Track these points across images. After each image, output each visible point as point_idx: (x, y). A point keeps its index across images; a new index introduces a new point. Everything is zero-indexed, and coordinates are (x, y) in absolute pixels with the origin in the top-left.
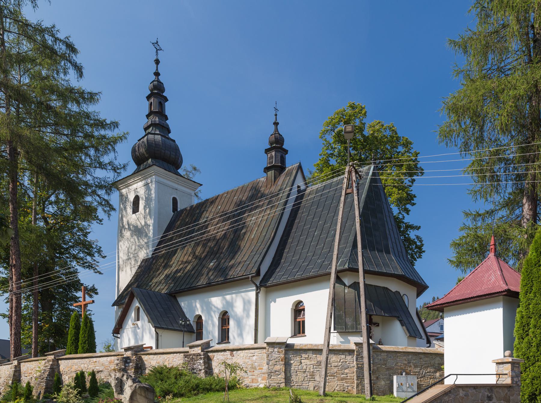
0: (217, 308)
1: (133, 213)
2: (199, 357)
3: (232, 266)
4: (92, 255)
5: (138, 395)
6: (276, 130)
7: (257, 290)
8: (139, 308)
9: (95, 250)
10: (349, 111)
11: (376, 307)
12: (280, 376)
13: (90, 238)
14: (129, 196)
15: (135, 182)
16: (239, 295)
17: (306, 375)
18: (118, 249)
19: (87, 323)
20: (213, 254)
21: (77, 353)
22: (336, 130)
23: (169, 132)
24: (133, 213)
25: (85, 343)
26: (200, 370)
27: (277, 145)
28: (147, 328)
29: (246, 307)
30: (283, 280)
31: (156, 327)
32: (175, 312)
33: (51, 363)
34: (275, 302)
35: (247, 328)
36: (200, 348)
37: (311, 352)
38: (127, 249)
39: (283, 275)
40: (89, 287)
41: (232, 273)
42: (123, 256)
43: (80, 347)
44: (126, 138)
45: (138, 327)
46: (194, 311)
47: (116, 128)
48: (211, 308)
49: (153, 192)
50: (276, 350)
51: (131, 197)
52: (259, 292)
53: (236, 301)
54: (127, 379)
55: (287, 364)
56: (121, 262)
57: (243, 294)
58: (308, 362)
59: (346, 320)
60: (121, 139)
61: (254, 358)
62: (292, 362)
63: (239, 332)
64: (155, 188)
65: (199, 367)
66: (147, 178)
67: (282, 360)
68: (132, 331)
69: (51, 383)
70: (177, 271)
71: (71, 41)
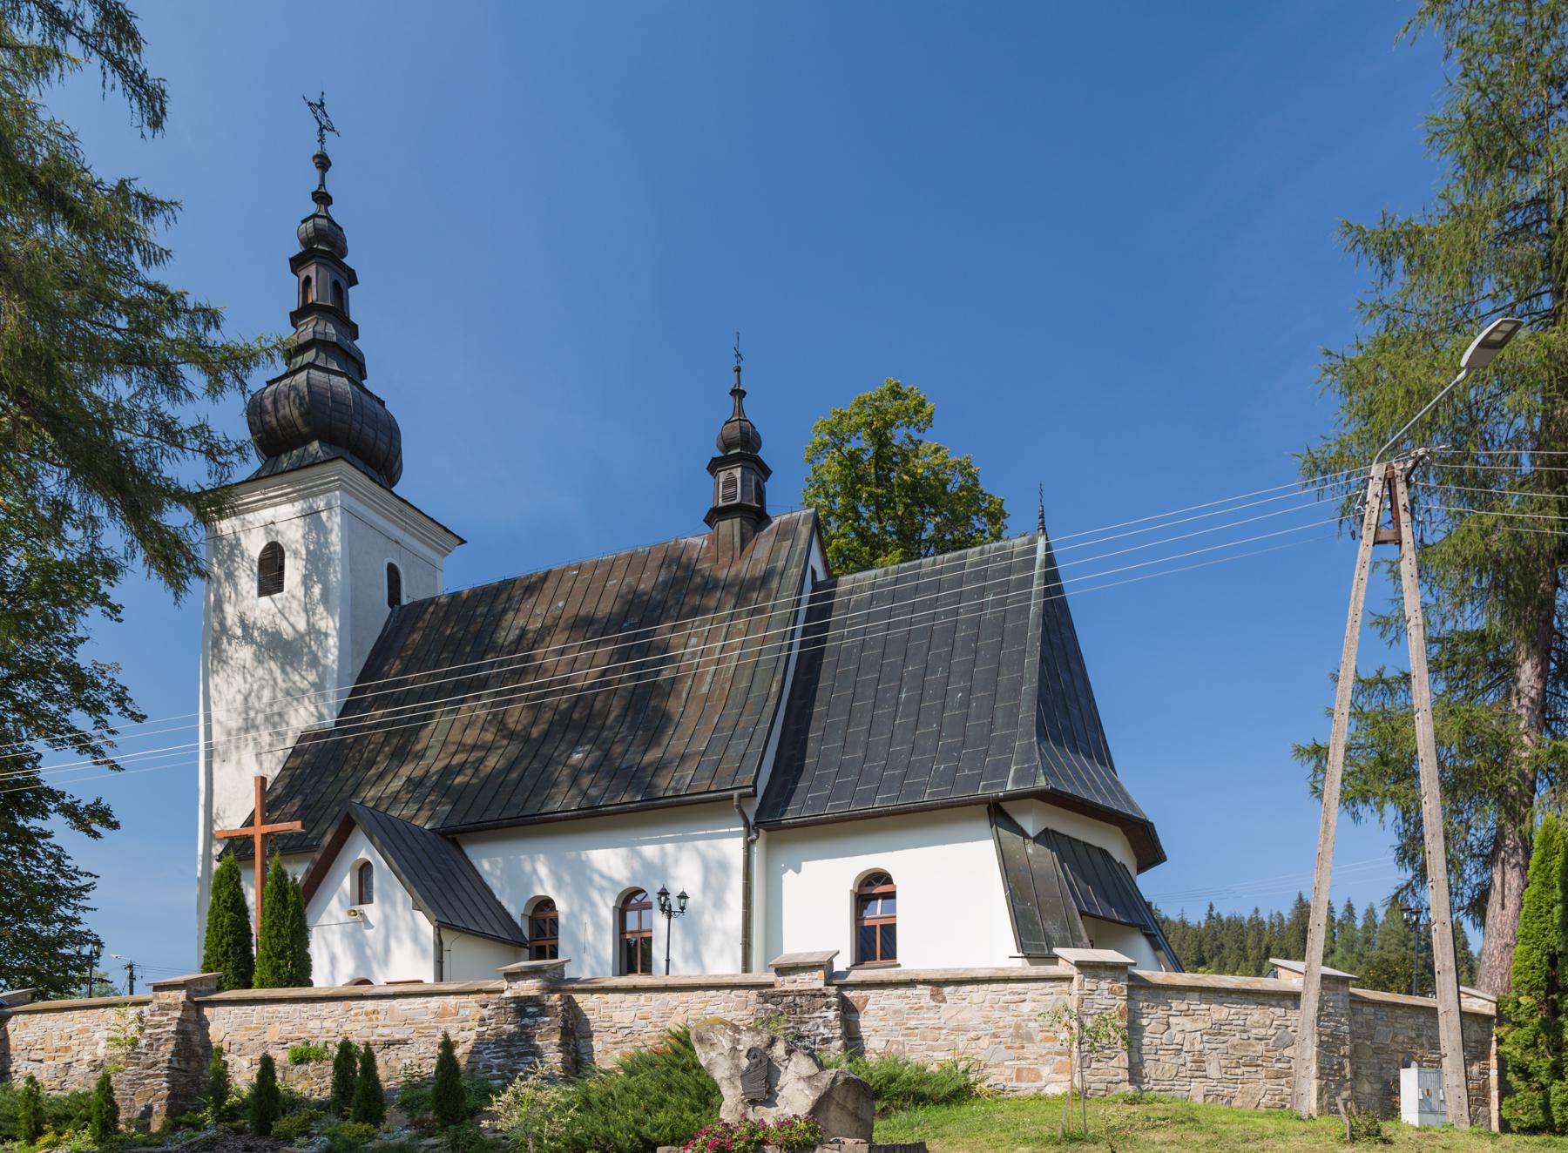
0: (611, 880)
1: (260, 595)
2: (820, 1001)
4: (95, 708)
5: (833, 1108)
9: (108, 694)
12: (1114, 1062)
14: (244, 542)
16: (689, 845)
17: (1181, 1061)
19: (286, 891)
21: (249, 985)
22: (845, 450)
24: (260, 595)
26: (826, 1041)
27: (743, 449)
28: (402, 924)
29: (713, 881)
30: (829, 810)
31: (440, 926)
33: (178, 1014)
34: (798, 870)
35: (717, 939)
36: (820, 974)
37: (1196, 995)
38: (240, 698)
39: (828, 798)
40: (82, 805)
41: (665, 784)
45: (366, 920)
46: (530, 886)
47: (213, 329)
48: (591, 881)
49: (335, 538)
50: (1104, 985)
51: (254, 545)
52: (753, 841)
53: (676, 861)
54: (789, 1052)
55: (1133, 1032)
56: (218, 735)
57: (701, 844)
58: (1187, 1024)
61: (1026, 1008)
63: (689, 948)
64: (342, 527)
65: (822, 1030)
66: (315, 495)
68: (343, 934)
69: (184, 1080)
70: (448, 771)
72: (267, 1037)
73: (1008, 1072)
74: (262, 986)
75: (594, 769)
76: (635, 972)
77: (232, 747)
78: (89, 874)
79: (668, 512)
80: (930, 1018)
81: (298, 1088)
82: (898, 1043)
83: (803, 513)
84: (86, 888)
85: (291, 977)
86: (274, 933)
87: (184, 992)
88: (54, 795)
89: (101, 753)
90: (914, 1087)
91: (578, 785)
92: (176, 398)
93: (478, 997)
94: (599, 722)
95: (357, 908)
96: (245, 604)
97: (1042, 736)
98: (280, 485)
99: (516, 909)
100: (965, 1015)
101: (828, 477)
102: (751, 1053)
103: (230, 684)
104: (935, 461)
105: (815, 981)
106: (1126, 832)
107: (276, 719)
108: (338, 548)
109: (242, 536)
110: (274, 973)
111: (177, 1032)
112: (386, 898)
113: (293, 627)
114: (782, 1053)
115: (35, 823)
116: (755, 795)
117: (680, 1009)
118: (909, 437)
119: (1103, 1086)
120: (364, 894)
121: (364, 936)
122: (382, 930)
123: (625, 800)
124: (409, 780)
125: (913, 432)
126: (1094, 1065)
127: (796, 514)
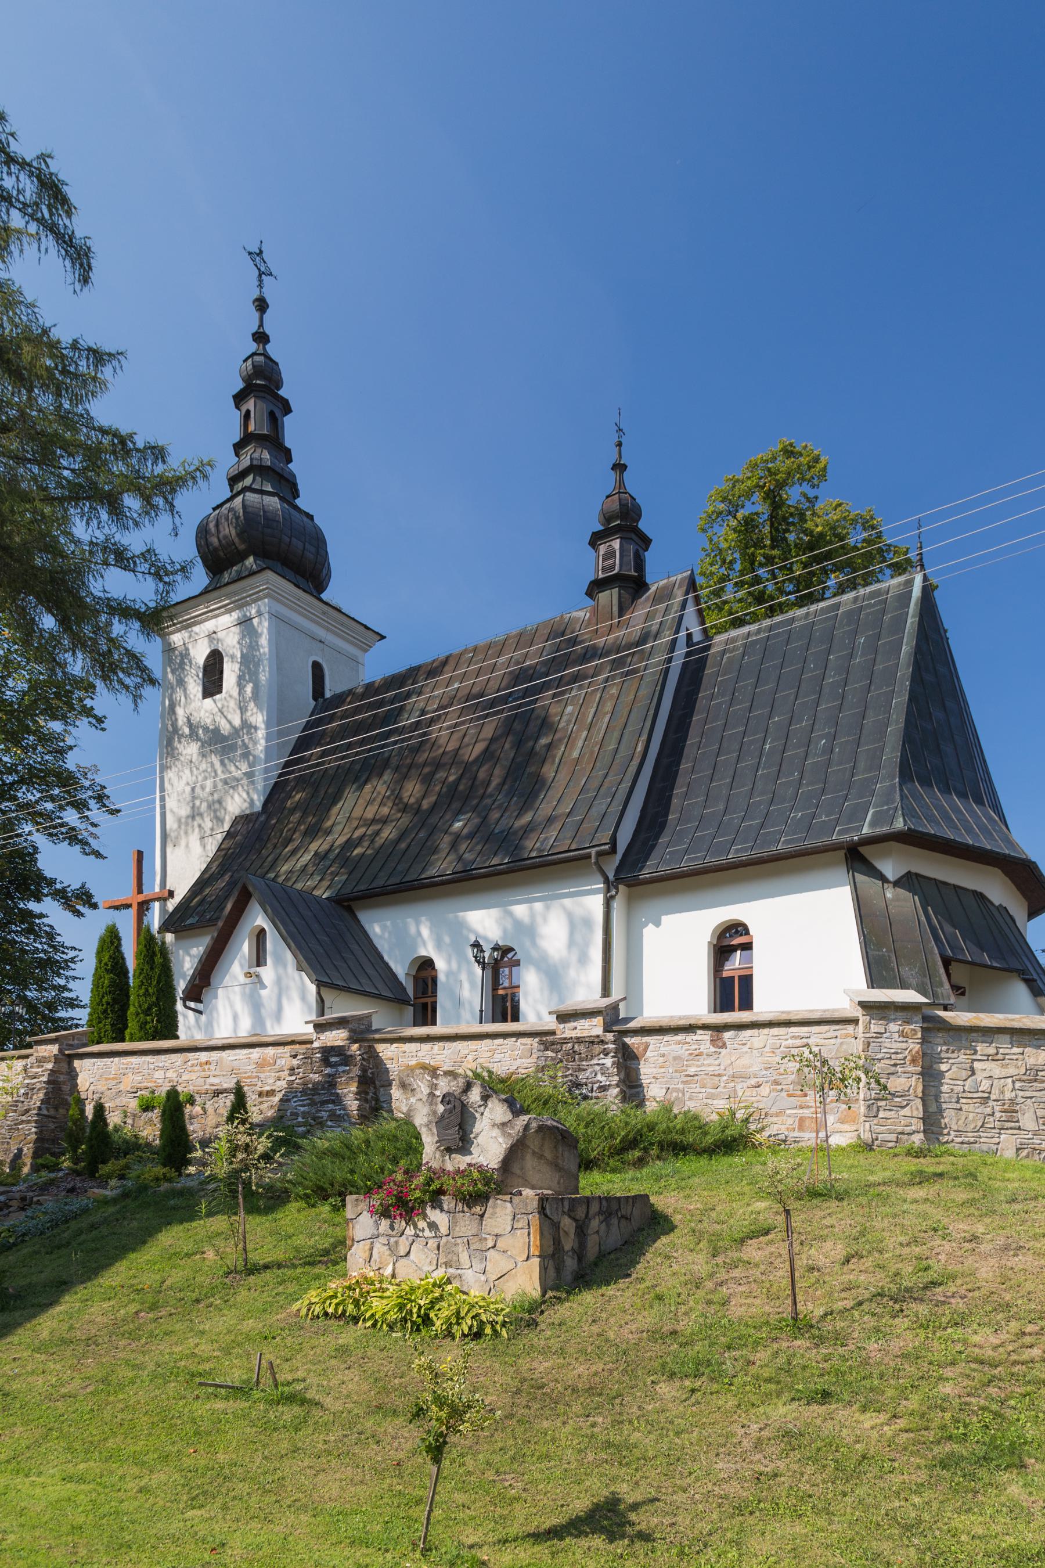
1: (204, 697)
3: (528, 829)
4: (80, 806)
5: (528, 1157)
6: (621, 483)
7: (608, 890)
8: (262, 931)
10: (784, 464)
11: (968, 942)
12: (906, 1111)
14: (192, 652)
16: (556, 903)
17: (988, 1111)
18: (162, 789)
19: (154, 954)
21: (123, 1040)
22: (740, 515)
23: (296, 494)
24: (204, 697)
25: (147, 1012)
26: (604, 1088)
27: (623, 522)
28: (292, 984)
30: (686, 864)
31: (320, 984)
32: (357, 947)
33: (50, 1066)
34: (658, 924)
36: (599, 1020)
37: (1007, 1037)
38: (188, 789)
39: (686, 852)
41: (532, 846)
42: (177, 806)
43: (133, 1025)
44: (205, 477)
46: (414, 947)
49: (264, 641)
50: (894, 1027)
51: (200, 654)
52: (612, 897)
53: (545, 920)
54: (485, 1098)
55: (930, 1076)
56: (171, 823)
57: (567, 902)
58: (995, 1069)
59: (902, 973)
60: (193, 478)
62: (943, 1067)
65: (599, 1077)
67: (913, 1061)
68: (243, 994)
69: (52, 1126)
70: (350, 845)
71: (52, 170)
72: (122, 1087)
73: (790, 1121)
74: (131, 1040)
75: (471, 836)
76: (506, 1021)
77: (182, 833)
79: (545, 585)
80: (709, 1065)
81: (144, 1134)
82: (677, 1090)
83: (680, 577)
86: (142, 992)
87: (57, 1046)
88: (51, 882)
89: (87, 844)
90: (678, 1138)
91: (456, 851)
92: (126, 528)
93: (288, 1048)
94: (481, 791)
95: (252, 971)
96: (193, 705)
97: (906, 774)
99: (401, 969)
100: (745, 1061)
101: (724, 545)
102: (446, 1099)
103: (180, 777)
104: (834, 516)
105: (594, 1027)
106: (1006, 873)
107: (217, 806)
108: (267, 650)
109: (190, 646)
110: (141, 1028)
111: (48, 1082)
112: (279, 961)
113: (230, 723)
114: (478, 1098)
115: (33, 906)
116: (613, 850)
117: (470, 1058)
118: (805, 495)
119: (893, 1137)
120: (260, 959)
121: (259, 996)
122: (276, 991)
124: (316, 854)
125: (806, 488)
126: (881, 1114)
127: (673, 579)
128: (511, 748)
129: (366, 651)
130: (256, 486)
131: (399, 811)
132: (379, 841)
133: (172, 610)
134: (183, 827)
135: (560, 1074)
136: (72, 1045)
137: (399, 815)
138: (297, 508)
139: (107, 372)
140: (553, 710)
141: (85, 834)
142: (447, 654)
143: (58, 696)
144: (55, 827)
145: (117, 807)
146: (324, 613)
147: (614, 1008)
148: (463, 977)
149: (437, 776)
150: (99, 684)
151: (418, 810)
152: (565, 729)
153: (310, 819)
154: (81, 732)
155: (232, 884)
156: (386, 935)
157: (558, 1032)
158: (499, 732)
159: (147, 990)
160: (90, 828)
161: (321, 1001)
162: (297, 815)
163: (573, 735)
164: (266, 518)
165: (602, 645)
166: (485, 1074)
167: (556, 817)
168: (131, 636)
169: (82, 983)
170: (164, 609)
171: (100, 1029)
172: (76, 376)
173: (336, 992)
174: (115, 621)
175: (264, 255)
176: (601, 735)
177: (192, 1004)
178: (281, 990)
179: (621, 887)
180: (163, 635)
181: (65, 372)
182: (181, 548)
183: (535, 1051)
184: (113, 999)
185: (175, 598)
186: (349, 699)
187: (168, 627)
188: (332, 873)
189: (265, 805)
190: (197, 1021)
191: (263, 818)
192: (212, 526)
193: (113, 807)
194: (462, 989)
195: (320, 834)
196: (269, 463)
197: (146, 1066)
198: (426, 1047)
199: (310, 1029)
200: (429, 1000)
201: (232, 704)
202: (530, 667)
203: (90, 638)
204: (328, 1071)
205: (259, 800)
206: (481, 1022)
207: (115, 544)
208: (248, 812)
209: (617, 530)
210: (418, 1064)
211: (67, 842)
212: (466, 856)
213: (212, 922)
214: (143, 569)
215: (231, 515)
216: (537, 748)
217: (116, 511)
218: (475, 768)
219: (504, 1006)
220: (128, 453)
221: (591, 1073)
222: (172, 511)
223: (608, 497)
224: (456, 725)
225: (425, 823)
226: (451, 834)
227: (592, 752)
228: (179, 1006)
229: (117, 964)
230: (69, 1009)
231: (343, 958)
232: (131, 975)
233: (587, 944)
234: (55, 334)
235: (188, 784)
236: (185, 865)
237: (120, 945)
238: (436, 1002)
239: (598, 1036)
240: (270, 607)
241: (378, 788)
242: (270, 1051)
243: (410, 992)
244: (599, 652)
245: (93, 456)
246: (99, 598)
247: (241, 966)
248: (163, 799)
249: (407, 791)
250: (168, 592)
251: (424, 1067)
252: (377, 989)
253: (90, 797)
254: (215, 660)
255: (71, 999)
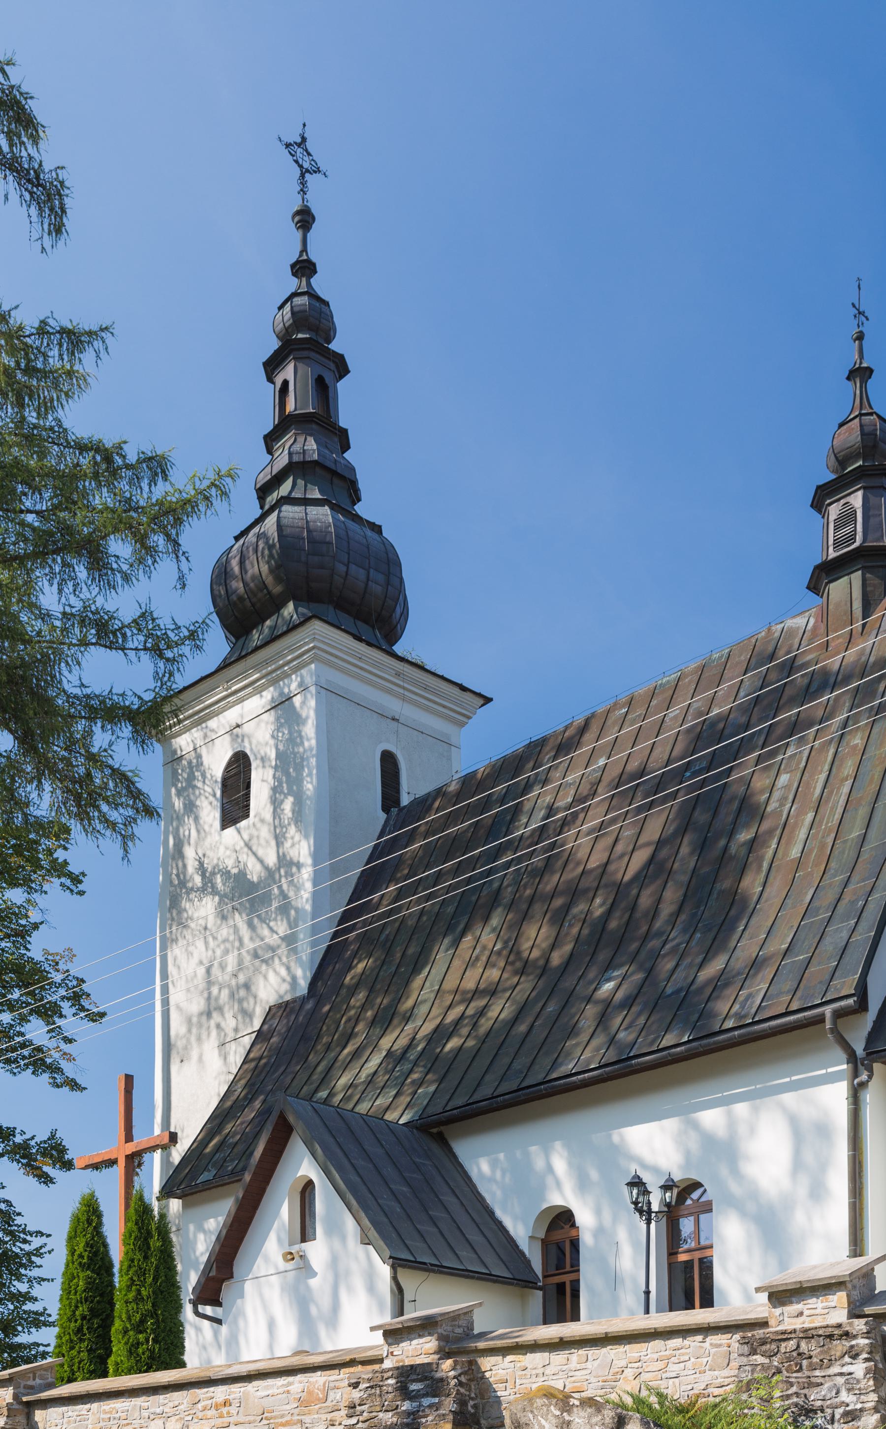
1: (224, 826)
2: (840, 1347)
3: (720, 983)
4: (48, 1013)
7: (856, 1074)
8: (309, 1185)
13: (37, 948)
14: (206, 760)
15: (236, 698)
18: (165, 975)
19: (149, 1234)
20: (603, 945)
21: (104, 1374)
23: (355, 496)
24: (224, 826)
25: (139, 1328)
28: (354, 1267)
31: (397, 1264)
32: (453, 1200)
36: (840, 1299)
38: (201, 971)
41: (727, 1010)
42: (185, 1000)
43: (119, 1348)
44: (224, 494)
46: (541, 1190)
49: (309, 730)
51: (216, 762)
52: (863, 1085)
53: (752, 1130)
56: (177, 1026)
57: (788, 1098)
60: (207, 498)
64: (317, 711)
65: (844, 1396)
68: (283, 1289)
70: (441, 1034)
74: (117, 1373)
75: (628, 1003)
76: (693, 1308)
77: (193, 1039)
78: (40, 1233)
84: (38, 1252)
85: (152, 1358)
86: (131, 1295)
89: (59, 1070)
91: (606, 1029)
93: (345, 1372)
94: (645, 928)
95: (294, 1249)
96: (208, 841)
98: (244, 674)
99: (521, 1229)
105: (832, 1310)
107: (242, 993)
108: (313, 742)
109: (204, 751)
110: (130, 1352)
113: (261, 861)
116: (862, 1005)
120: (306, 1232)
121: (308, 1288)
122: (330, 1278)
123: (665, 1043)
124: (389, 1053)
128: (692, 853)
129: (462, 725)
130: (297, 494)
131: (515, 973)
132: (485, 1025)
133: (176, 701)
134: (194, 1030)
135: (777, 1393)
136: (32, 1387)
137: (516, 979)
138: (357, 518)
139: (87, 361)
140: (760, 782)
141: (56, 1055)
142: (588, 713)
143: (18, 850)
144: (14, 1049)
145: (101, 1009)
146: (398, 674)
147: (867, 1275)
148: (622, 1235)
149: (575, 910)
150: (75, 826)
151: (545, 969)
152: (777, 813)
153: (379, 1000)
154: (50, 903)
155: (264, 1114)
156: (498, 1175)
157: (772, 1322)
158: (671, 829)
159: (139, 1292)
160: (63, 1046)
161: (398, 1290)
162: (361, 996)
163: (791, 821)
164: (312, 541)
165: (836, 667)
166: (653, 1399)
167: (766, 960)
168: (116, 745)
169: (48, 1289)
170: (167, 699)
171: (72, 1359)
172: (45, 374)
173: (422, 1275)
174: (97, 729)
175: (308, 144)
176: (837, 816)
177: (208, 1310)
178: (338, 1275)
179: (877, 1066)
180: (164, 738)
181: (30, 371)
182: (194, 605)
183: (734, 1356)
184: (91, 1310)
185: (181, 681)
186: (436, 804)
187: (171, 727)
188: (413, 1082)
189: (312, 985)
190: (216, 1334)
191: (309, 1006)
192: (235, 564)
193: (95, 1010)
194: (620, 1257)
195: (395, 1021)
196: (315, 457)
197: (137, 1415)
198: (558, 1358)
199: (378, 1338)
200: (567, 1279)
201: (265, 832)
202: (720, 718)
203: (63, 759)
204: (406, 1406)
205: (304, 977)
206: (647, 1311)
207: (97, 612)
208: (288, 998)
209: (859, 475)
210: (539, 1389)
211: (29, 1071)
212: (621, 1035)
213: (235, 1176)
214: (136, 644)
215: (261, 545)
216: (733, 849)
217: (99, 563)
218: (634, 892)
219: (689, 1281)
220: (114, 473)
221: (830, 1390)
222: (176, 552)
223: (841, 425)
224: (602, 826)
225: (556, 988)
226: (597, 1002)
227: (823, 846)
228: (188, 1311)
229: (96, 1254)
230: (33, 1330)
231: (431, 1218)
232: (116, 1270)
233: (823, 1166)
234: (17, 318)
235: (201, 963)
236: (195, 1089)
237: (100, 1224)
238: (578, 1281)
239: (839, 1326)
240: (318, 676)
241: (484, 938)
242: (319, 1378)
243: (537, 1266)
244: (832, 680)
245: (67, 486)
246: (76, 697)
247: (279, 1240)
248: (165, 990)
249: (528, 939)
250: (171, 674)
251: (549, 1394)
252: (487, 1268)
253: (63, 998)
254: (239, 769)
255: (36, 1313)
